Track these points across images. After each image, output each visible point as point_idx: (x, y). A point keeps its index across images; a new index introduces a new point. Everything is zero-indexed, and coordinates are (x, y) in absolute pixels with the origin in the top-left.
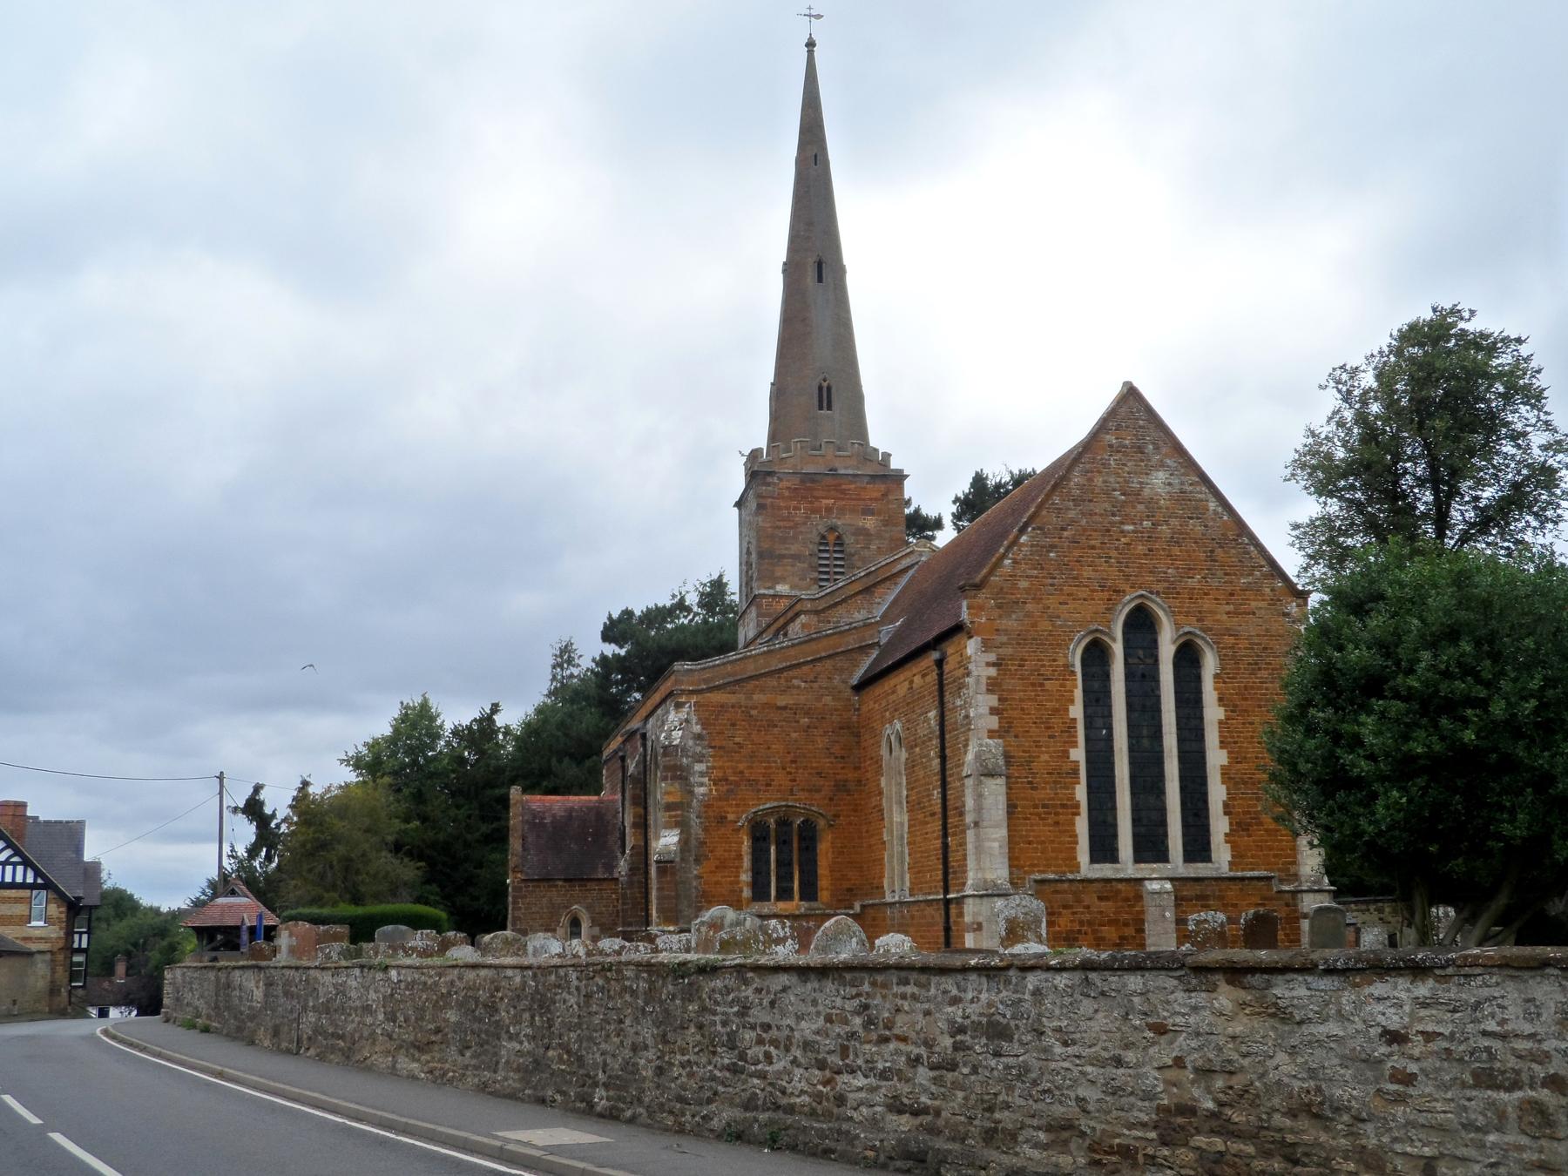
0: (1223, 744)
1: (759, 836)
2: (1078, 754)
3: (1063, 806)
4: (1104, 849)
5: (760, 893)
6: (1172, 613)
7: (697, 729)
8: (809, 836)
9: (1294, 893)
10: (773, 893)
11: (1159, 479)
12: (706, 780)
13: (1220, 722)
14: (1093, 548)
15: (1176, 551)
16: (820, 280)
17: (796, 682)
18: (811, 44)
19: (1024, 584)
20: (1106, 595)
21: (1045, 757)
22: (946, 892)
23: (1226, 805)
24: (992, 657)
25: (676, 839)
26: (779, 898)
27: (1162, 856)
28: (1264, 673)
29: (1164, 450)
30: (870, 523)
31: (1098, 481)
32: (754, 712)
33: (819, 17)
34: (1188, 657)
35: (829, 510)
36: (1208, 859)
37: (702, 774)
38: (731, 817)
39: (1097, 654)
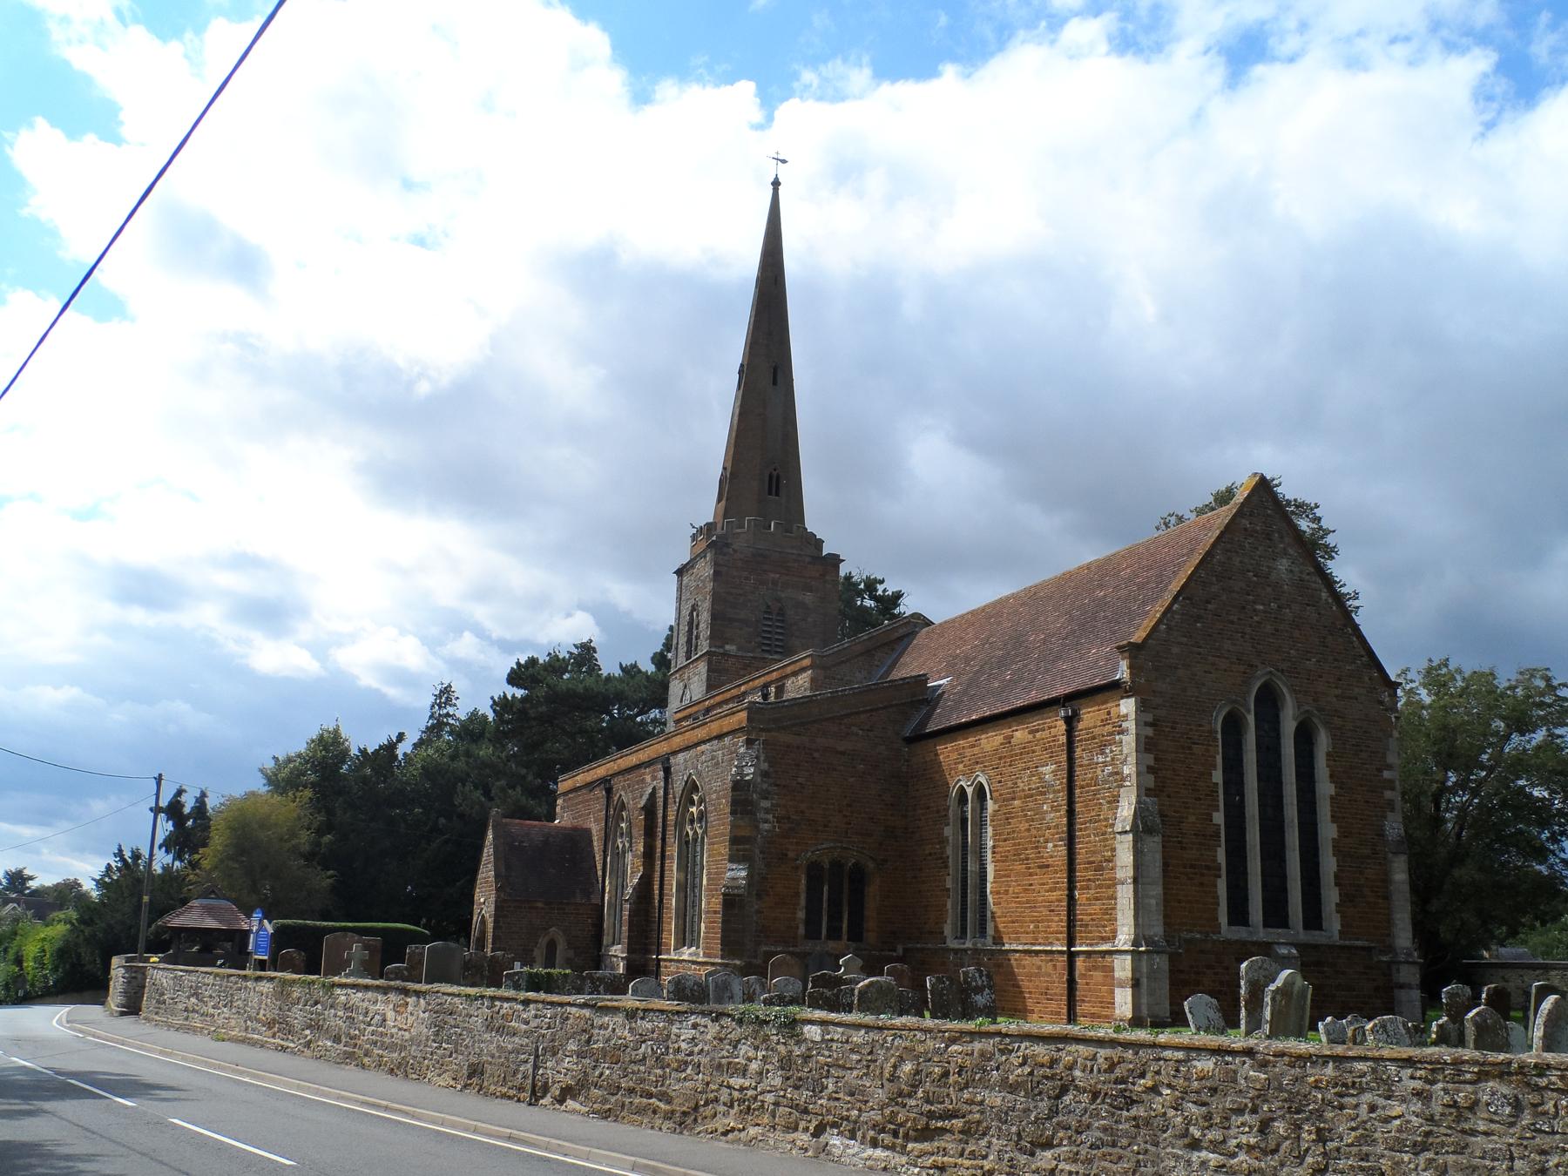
0: (1334, 818)
1: (815, 873)
2: (1219, 818)
3: (1208, 868)
4: (1239, 915)
5: (813, 933)
6: (1293, 691)
7: (765, 766)
8: (858, 878)
9: (1389, 964)
10: (824, 932)
11: (1283, 565)
12: (770, 817)
13: (1332, 798)
14: (1232, 622)
15: (1296, 633)
16: (775, 383)
17: (854, 729)
18: (776, 184)
19: (1175, 650)
20: (1242, 668)
21: (1192, 819)
22: (1071, 942)
23: (1336, 876)
24: (1149, 718)
25: (744, 874)
26: (829, 937)
27: (1284, 923)
28: (1363, 755)
29: (1286, 540)
30: (808, 598)
31: (1236, 560)
32: (816, 755)
33: (784, 161)
34: (1305, 737)
35: (775, 583)
36: (1320, 928)
37: (767, 811)
38: (791, 855)
39: (1233, 725)
